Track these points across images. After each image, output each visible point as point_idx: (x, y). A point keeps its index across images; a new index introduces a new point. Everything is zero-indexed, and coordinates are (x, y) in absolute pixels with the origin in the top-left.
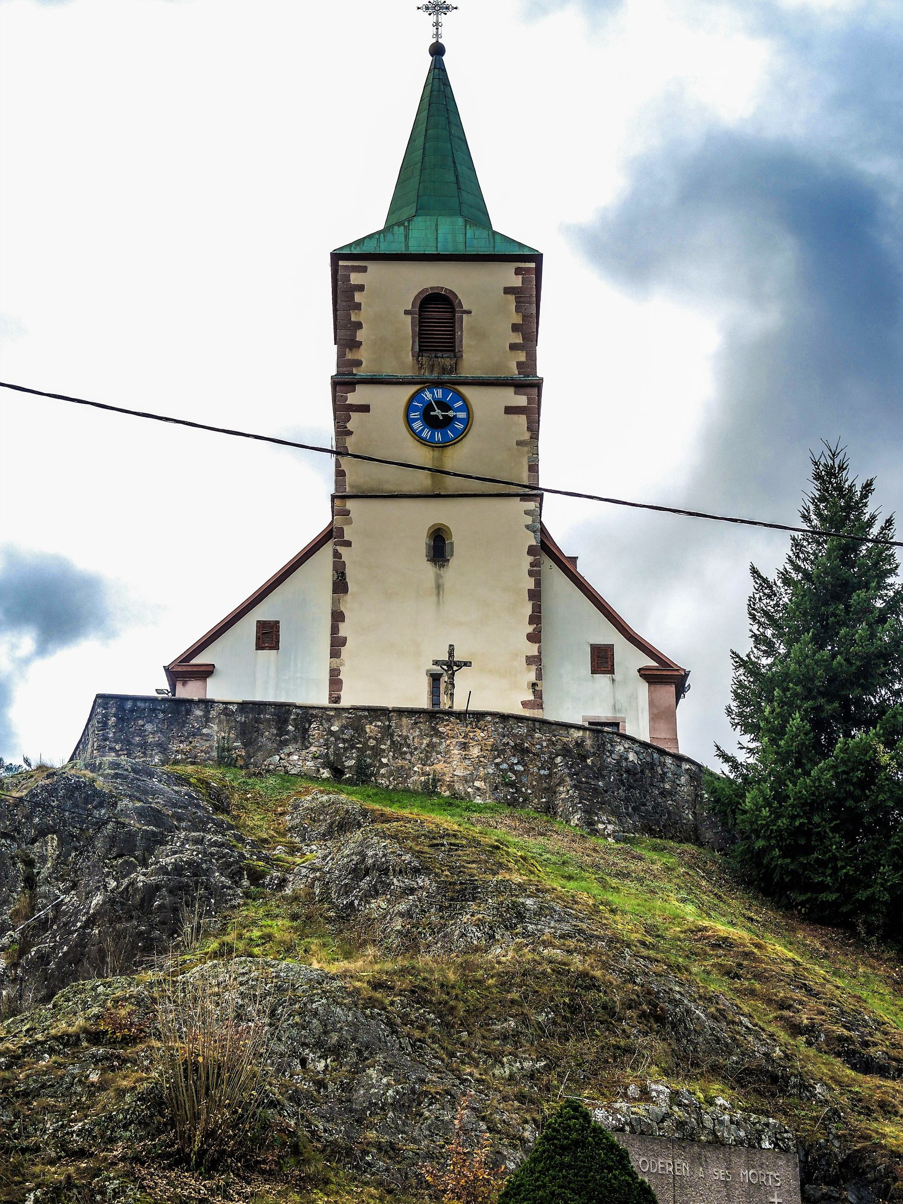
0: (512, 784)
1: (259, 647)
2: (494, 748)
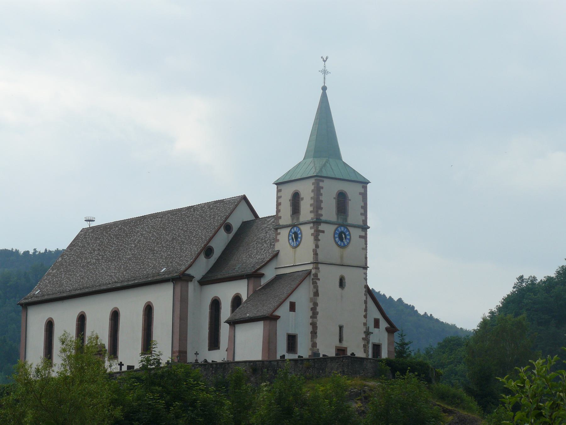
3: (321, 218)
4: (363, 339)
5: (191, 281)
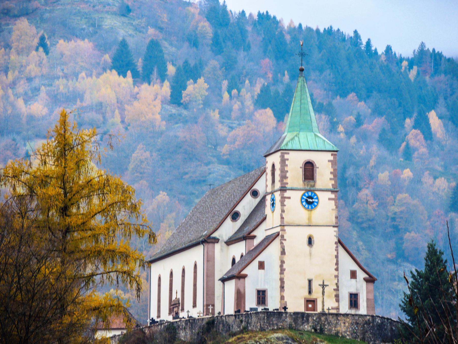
0: (356, 333)
1: (259, 269)
2: (351, 323)
3: (286, 186)
4: (334, 290)
5: (218, 242)
